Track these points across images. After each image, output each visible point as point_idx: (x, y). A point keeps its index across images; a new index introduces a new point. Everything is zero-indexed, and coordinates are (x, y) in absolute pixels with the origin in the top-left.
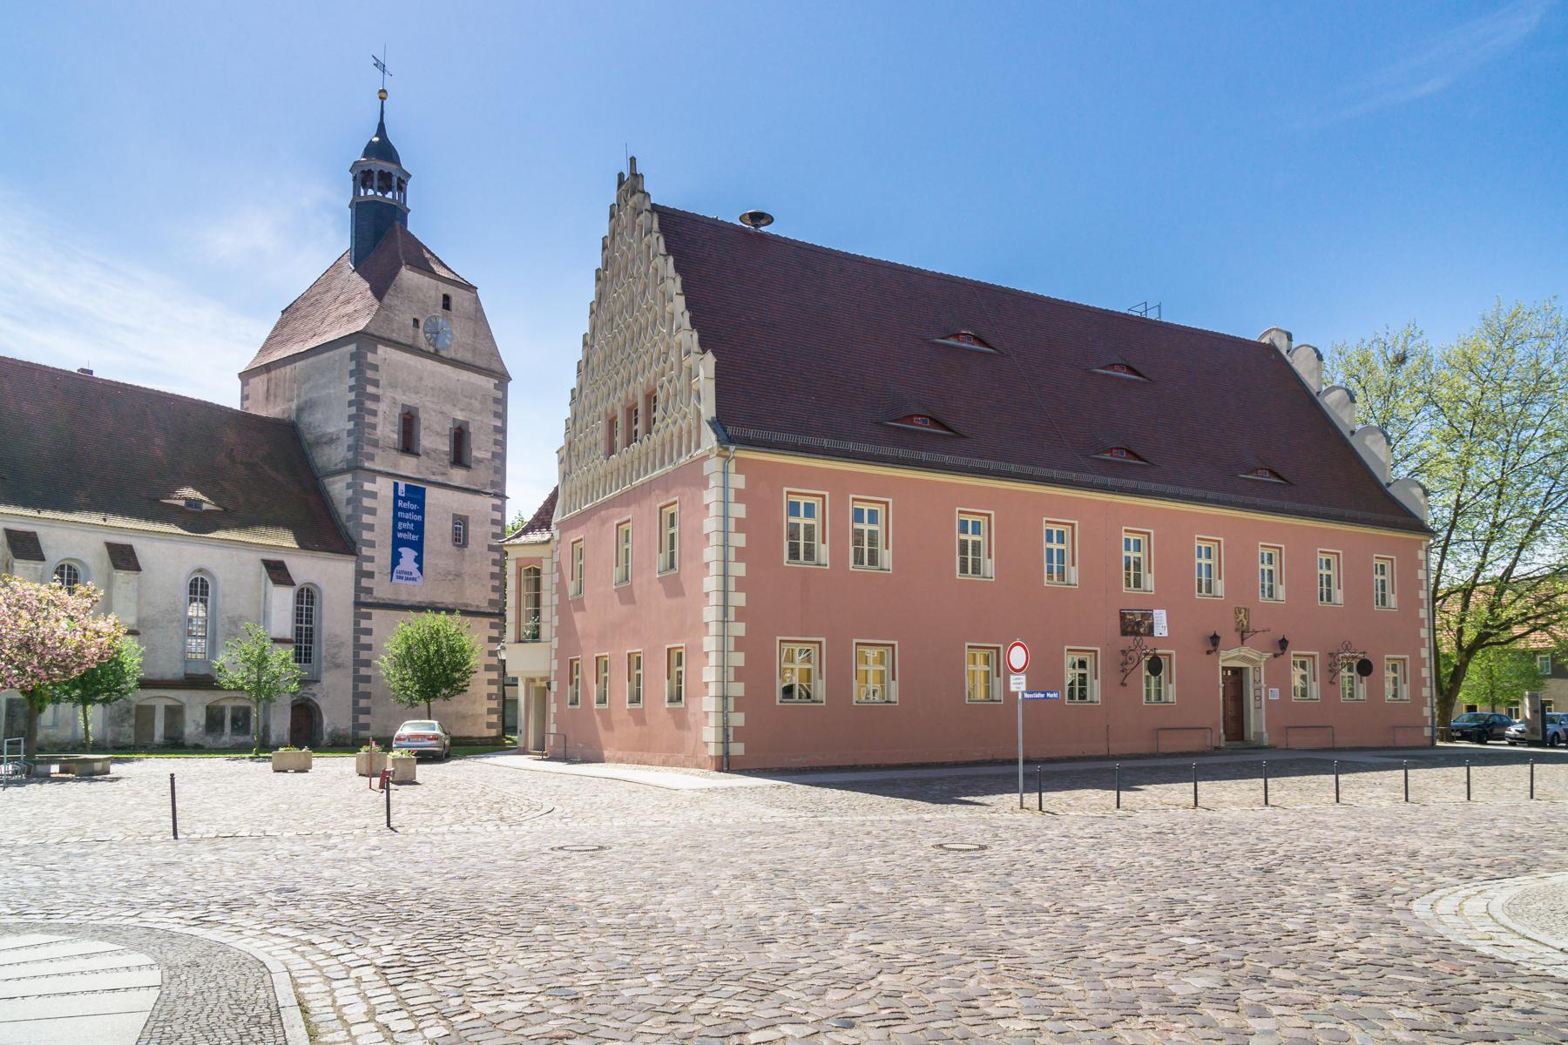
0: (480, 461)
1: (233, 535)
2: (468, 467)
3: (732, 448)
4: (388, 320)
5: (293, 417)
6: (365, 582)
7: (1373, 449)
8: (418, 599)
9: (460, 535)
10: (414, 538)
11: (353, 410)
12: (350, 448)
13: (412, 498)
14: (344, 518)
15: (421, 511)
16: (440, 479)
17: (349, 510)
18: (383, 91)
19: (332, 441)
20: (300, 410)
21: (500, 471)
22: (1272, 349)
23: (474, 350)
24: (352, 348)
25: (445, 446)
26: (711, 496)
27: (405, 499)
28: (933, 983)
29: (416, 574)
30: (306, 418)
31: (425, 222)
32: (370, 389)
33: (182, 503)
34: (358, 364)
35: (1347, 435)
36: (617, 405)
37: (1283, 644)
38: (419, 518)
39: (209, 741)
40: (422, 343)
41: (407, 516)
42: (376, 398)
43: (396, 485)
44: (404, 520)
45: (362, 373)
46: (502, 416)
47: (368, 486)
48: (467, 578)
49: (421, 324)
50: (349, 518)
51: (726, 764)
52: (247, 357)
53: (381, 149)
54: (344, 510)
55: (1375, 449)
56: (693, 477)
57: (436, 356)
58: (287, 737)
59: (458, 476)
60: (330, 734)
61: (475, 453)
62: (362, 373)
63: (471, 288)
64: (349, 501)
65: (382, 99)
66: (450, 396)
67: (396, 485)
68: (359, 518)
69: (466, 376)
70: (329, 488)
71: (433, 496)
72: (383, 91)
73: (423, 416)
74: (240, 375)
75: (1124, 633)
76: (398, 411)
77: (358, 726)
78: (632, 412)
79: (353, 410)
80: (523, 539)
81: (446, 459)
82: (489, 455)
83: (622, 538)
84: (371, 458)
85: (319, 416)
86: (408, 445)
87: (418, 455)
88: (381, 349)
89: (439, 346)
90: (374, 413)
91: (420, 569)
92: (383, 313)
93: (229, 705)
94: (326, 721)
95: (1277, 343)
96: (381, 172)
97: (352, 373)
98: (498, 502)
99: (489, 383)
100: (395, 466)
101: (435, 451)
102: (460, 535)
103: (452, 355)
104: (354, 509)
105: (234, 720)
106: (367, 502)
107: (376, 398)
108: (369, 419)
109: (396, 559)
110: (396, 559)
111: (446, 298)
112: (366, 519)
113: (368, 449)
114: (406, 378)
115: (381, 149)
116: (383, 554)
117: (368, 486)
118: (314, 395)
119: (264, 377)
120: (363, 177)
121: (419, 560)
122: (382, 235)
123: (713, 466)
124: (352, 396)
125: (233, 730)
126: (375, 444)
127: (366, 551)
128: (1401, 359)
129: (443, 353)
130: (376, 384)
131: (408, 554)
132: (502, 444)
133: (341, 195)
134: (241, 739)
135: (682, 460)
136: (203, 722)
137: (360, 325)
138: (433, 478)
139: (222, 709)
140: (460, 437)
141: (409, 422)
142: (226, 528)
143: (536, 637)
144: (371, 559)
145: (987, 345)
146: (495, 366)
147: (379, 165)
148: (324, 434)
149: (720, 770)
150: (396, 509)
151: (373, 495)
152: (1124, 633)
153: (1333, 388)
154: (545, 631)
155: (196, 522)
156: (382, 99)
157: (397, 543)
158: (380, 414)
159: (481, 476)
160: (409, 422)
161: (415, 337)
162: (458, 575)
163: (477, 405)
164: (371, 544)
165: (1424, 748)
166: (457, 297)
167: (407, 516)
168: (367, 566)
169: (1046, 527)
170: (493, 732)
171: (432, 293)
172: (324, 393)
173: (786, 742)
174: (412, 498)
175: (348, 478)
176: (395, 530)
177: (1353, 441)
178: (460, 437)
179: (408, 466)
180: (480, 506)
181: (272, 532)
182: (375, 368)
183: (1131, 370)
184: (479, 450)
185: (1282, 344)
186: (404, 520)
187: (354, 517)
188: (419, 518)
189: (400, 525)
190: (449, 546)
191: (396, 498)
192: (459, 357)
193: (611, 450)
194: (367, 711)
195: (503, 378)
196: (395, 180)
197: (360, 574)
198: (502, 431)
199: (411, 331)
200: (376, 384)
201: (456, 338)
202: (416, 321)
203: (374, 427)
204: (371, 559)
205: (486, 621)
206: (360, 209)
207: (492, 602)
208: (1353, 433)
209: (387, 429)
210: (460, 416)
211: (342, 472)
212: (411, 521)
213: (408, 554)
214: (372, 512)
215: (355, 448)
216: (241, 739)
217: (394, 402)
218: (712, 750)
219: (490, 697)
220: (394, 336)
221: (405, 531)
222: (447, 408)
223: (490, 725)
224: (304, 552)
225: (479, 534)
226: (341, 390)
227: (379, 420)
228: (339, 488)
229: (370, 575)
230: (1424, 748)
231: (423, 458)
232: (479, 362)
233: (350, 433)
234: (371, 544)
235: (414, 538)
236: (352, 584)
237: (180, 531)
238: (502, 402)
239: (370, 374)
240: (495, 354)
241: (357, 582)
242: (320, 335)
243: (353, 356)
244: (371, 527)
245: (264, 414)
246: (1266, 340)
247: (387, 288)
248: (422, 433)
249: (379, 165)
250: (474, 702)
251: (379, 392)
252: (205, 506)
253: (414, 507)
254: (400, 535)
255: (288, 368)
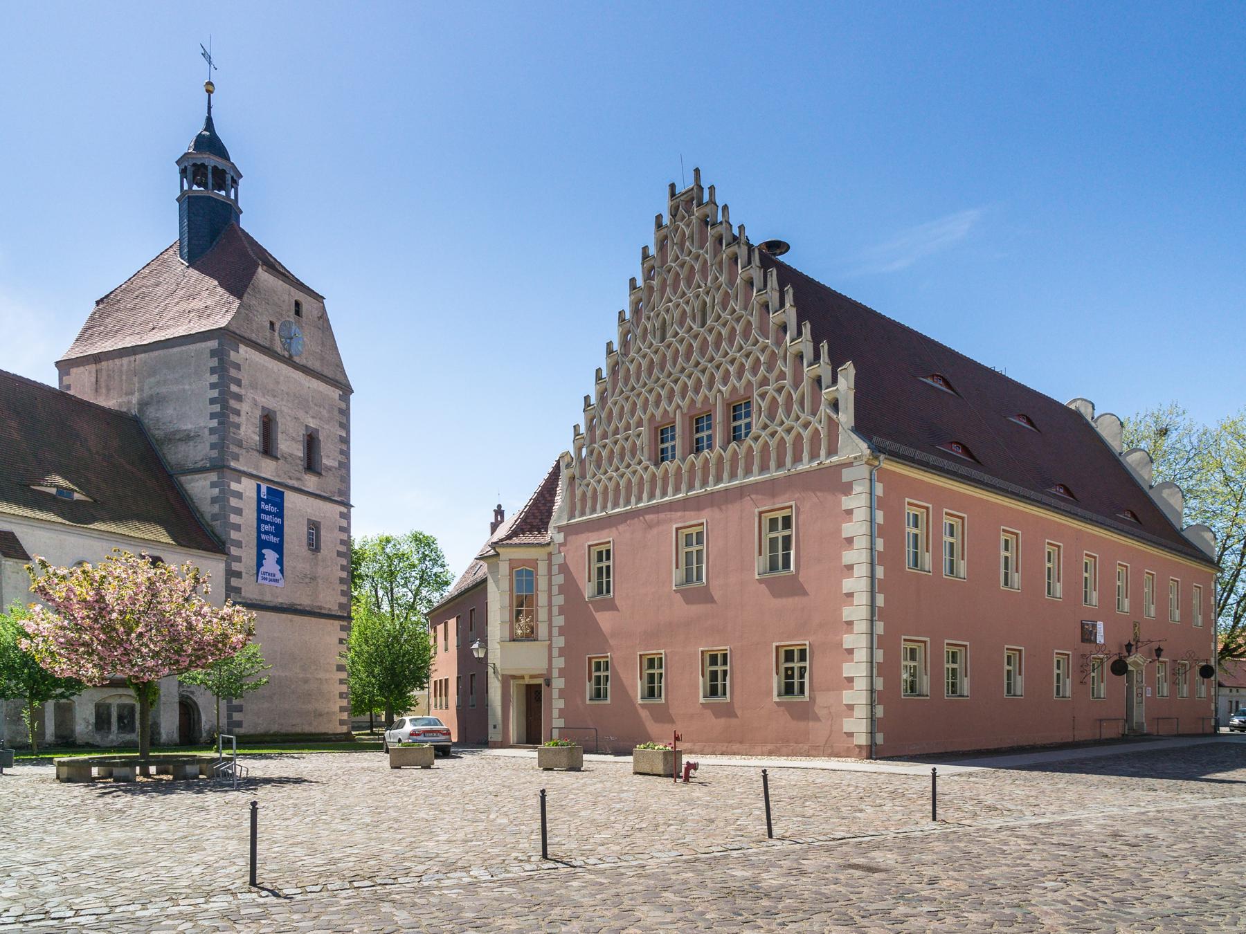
0: (329, 469)
1: (111, 527)
2: (319, 474)
3: (882, 457)
4: (248, 320)
5: (134, 411)
6: (235, 582)
7: (1169, 500)
8: (280, 600)
9: (314, 543)
10: (276, 540)
11: (217, 408)
12: (213, 446)
13: (273, 499)
14: (208, 517)
15: (280, 515)
16: (295, 484)
17: (216, 509)
18: (210, 83)
19: (188, 438)
20: (143, 405)
21: (346, 480)
22: (1076, 416)
23: (322, 359)
24: (214, 344)
25: (299, 452)
26: (857, 501)
27: (267, 502)
28: (219, 923)
29: (279, 576)
30: (152, 413)
31: (257, 221)
32: (234, 388)
33: (53, 491)
34: (221, 360)
35: (1146, 488)
36: (677, 410)
37: (1159, 651)
38: (278, 521)
39: (97, 739)
40: (278, 348)
41: (269, 518)
42: (239, 398)
43: (259, 487)
44: (266, 523)
45: (223, 369)
46: (346, 426)
47: (234, 486)
48: (320, 581)
49: (277, 327)
50: (215, 517)
51: (873, 752)
52: (64, 349)
53: (209, 142)
54: (208, 510)
55: (1172, 501)
56: (831, 482)
57: (289, 361)
58: (176, 736)
59: (311, 482)
60: (207, 727)
61: (325, 461)
62: (223, 369)
63: (319, 298)
64: (214, 500)
65: (209, 92)
66: (302, 402)
67: (259, 487)
68: (226, 517)
69: (316, 384)
70: (188, 487)
71: (290, 499)
72: (210, 83)
73: (280, 419)
74: (58, 364)
75: (1083, 640)
76: (258, 413)
77: (232, 724)
78: (699, 421)
79: (217, 408)
80: (515, 540)
81: (301, 464)
82: (336, 464)
83: (682, 541)
84: (236, 457)
85: (170, 411)
86: (268, 448)
87: (276, 458)
88: (243, 349)
89: (293, 352)
90: (238, 413)
91: (282, 571)
92: (242, 310)
93: (115, 702)
94: (204, 718)
95: (1082, 410)
96: (215, 168)
97: (213, 371)
98: (344, 510)
99: (335, 394)
100: (257, 467)
101: (291, 455)
102: (314, 543)
103: (304, 362)
104: (223, 508)
105: (120, 718)
106: (233, 502)
107: (239, 398)
108: (233, 418)
109: (260, 558)
110: (260, 558)
111: (297, 304)
112: (233, 518)
113: (234, 449)
114: (266, 382)
115: (209, 142)
116: (248, 554)
117: (234, 486)
118: (163, 390)
119: (93, 367)
120: (192, 170)
121: (280, 562)
122: (213, 231)
123: (858, 475)
124: (215, 393)
125: (119, 728)
126: (239, 444)
127: (234, 551)
128: (1164, 432)
129: (296, 359)
130: (238, 383)
131: (270, 556)
132: (346, 453)
133: (171, 185)
134: (128, 737)
135: (800, 468)
136: (92, 720)
137: (223, 323)
138: (291, 482)
139: (109, 706)
140: (311, 442)
141: (268, 424)
142: (103, 520)
143: (531, 636)
144: (239, 559)
145: (950, 387)
146: (339, 377)
147: (211, 160)
148: (179, 431)
149: (870, 757)
150: (260, 511)
151: (239, 495)
152: (1083, 640)
153: (1135, 450)
154: (542, 630)
155: (78, 515)
156: (209, 92)
157: (261, 545)
158: (243, 413)
159: (329, 484)
160: (268, 424)
161: (272, 340)
162: (314, 579)
163: (325, 413)
164: (238, 544)
165: (1205, 735)
166: (306, 305)
167: (269, 518)
168: (236, 566)
169: (1048, 549)
170: (344, 729)
171: (286, 297)
172: (175, 388)
173: (913, 730)
174: (273, 499)
175: (213, 477)
176: (259, 532)
177: (1151, 494)
178: (311, 442)
179: (268, 468)
180: (327, 512)
181: (145, 526)
182: (238, 367)
183: (1030, 422)
184: (328, 459)
185: (1086, 411)
186: (266, 523)
187: (223, 516)
188: (278, 521)
189: (264, 527)
190: (304, 551)
191: (259, 500)
192: (309, 364)
193: (661, 457)
194: (240, 709)
195: (346, 390)
196: (229, 178)
197: (230, 574)
198: (346, 441)
199: (268, 333)
200: (238, 383)
201: (306, 345)
202: (272, 324)
203: (238, 426)
204: (239, 559)
205: (337, 623)
206: (189, 204)
207: (341, 606)
208: (1151, 487)
209: (249, 431)
210: (312, 424)
211: (203, 470)
212: (272, 524)
213: (270, 556)
214: (239, 512)
215: (221, 446)
216: (128, 737)
217: (255, 403)
218: (862, 740)
219: (341, 695)
220: (254, 337)
221: (267, 533)
222: (301, 414)
223: (342, 722)
224: (179, 549)
225: (329, 538)
226: (202, 386)
227: (242, 420)
228: (200, 488)
229: (238, 575)
230: (1205, 735)
231: (281, 461)
232: (326, 372)
233: (212, 431)
234: (238, 544)
235: (276, 540)
236: (223, 584)
237: (60, 520)
238: (345, 412)
239: (233, 372)
240: (339, 366)
241: (228, 582)
242: (161, 328)
243: (213, 353)
244: (237, 528)
245: (102, 404)
246: (1072, 407)
247: (246, 286)
248: (280, 436)
249: (211, 160)
250: (328, 701)
251: (242, 392)
252: (77, 496)
253: (274, 510)
254: (263, 537)
255: (125, 360)
